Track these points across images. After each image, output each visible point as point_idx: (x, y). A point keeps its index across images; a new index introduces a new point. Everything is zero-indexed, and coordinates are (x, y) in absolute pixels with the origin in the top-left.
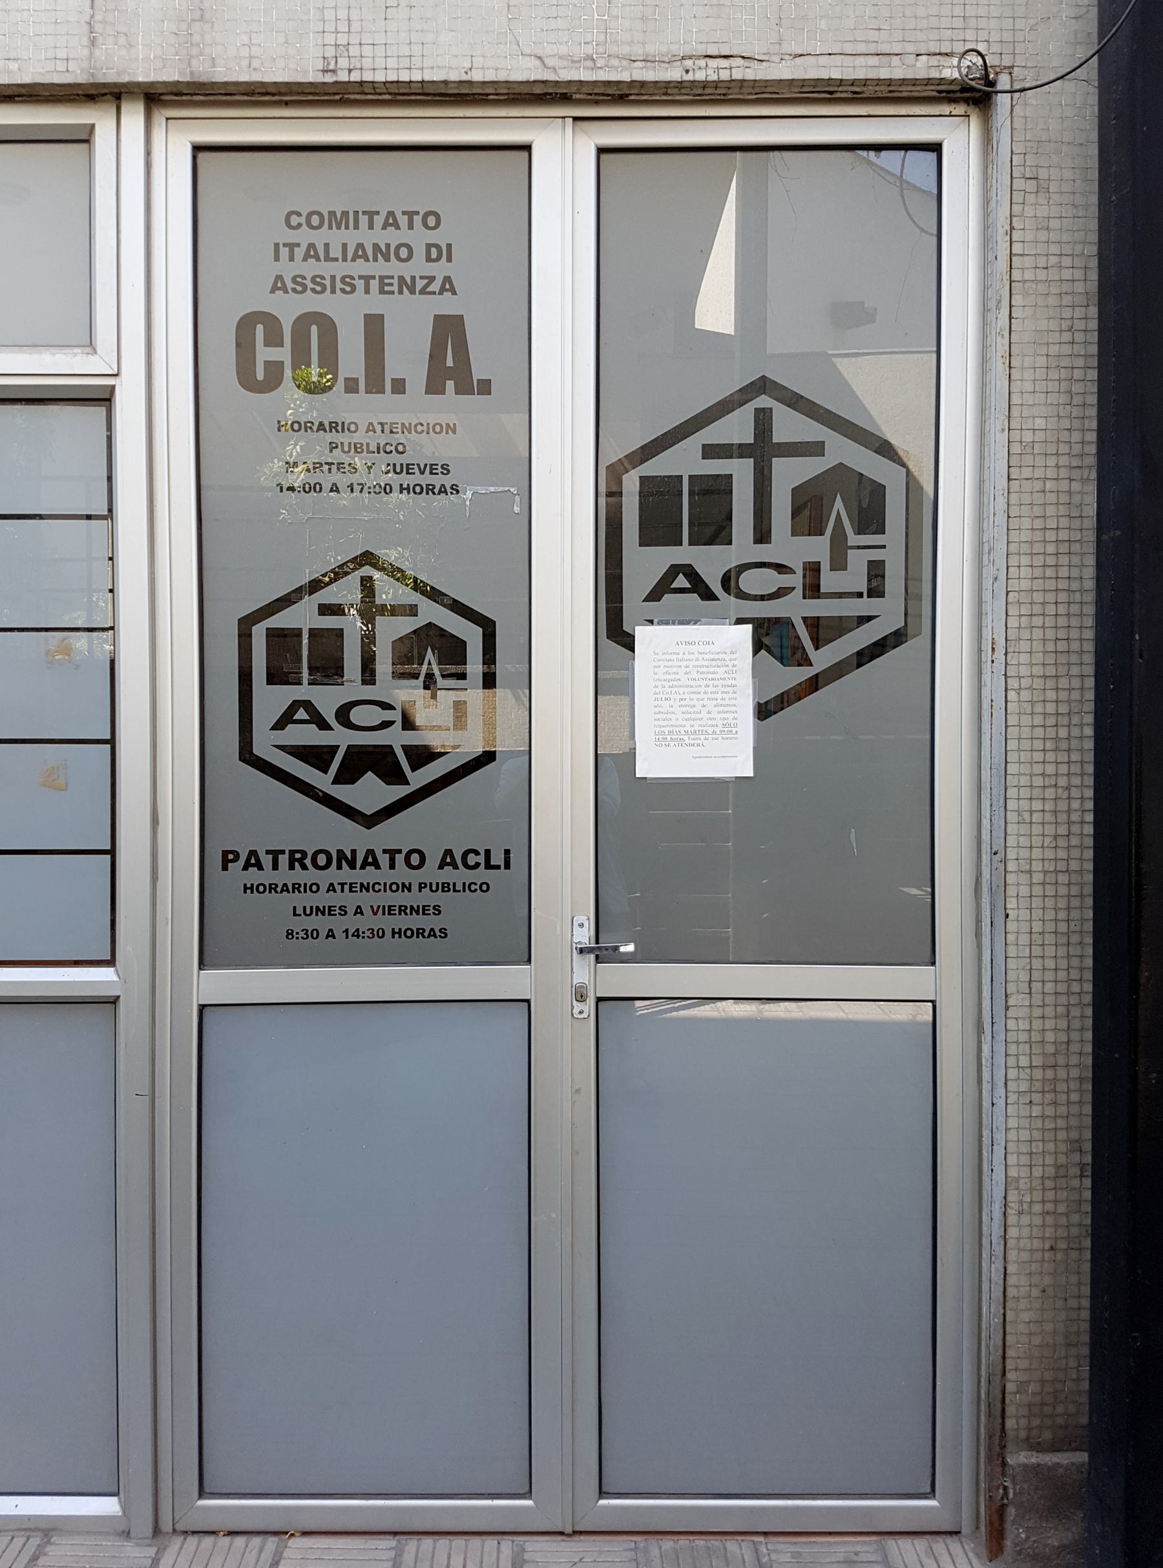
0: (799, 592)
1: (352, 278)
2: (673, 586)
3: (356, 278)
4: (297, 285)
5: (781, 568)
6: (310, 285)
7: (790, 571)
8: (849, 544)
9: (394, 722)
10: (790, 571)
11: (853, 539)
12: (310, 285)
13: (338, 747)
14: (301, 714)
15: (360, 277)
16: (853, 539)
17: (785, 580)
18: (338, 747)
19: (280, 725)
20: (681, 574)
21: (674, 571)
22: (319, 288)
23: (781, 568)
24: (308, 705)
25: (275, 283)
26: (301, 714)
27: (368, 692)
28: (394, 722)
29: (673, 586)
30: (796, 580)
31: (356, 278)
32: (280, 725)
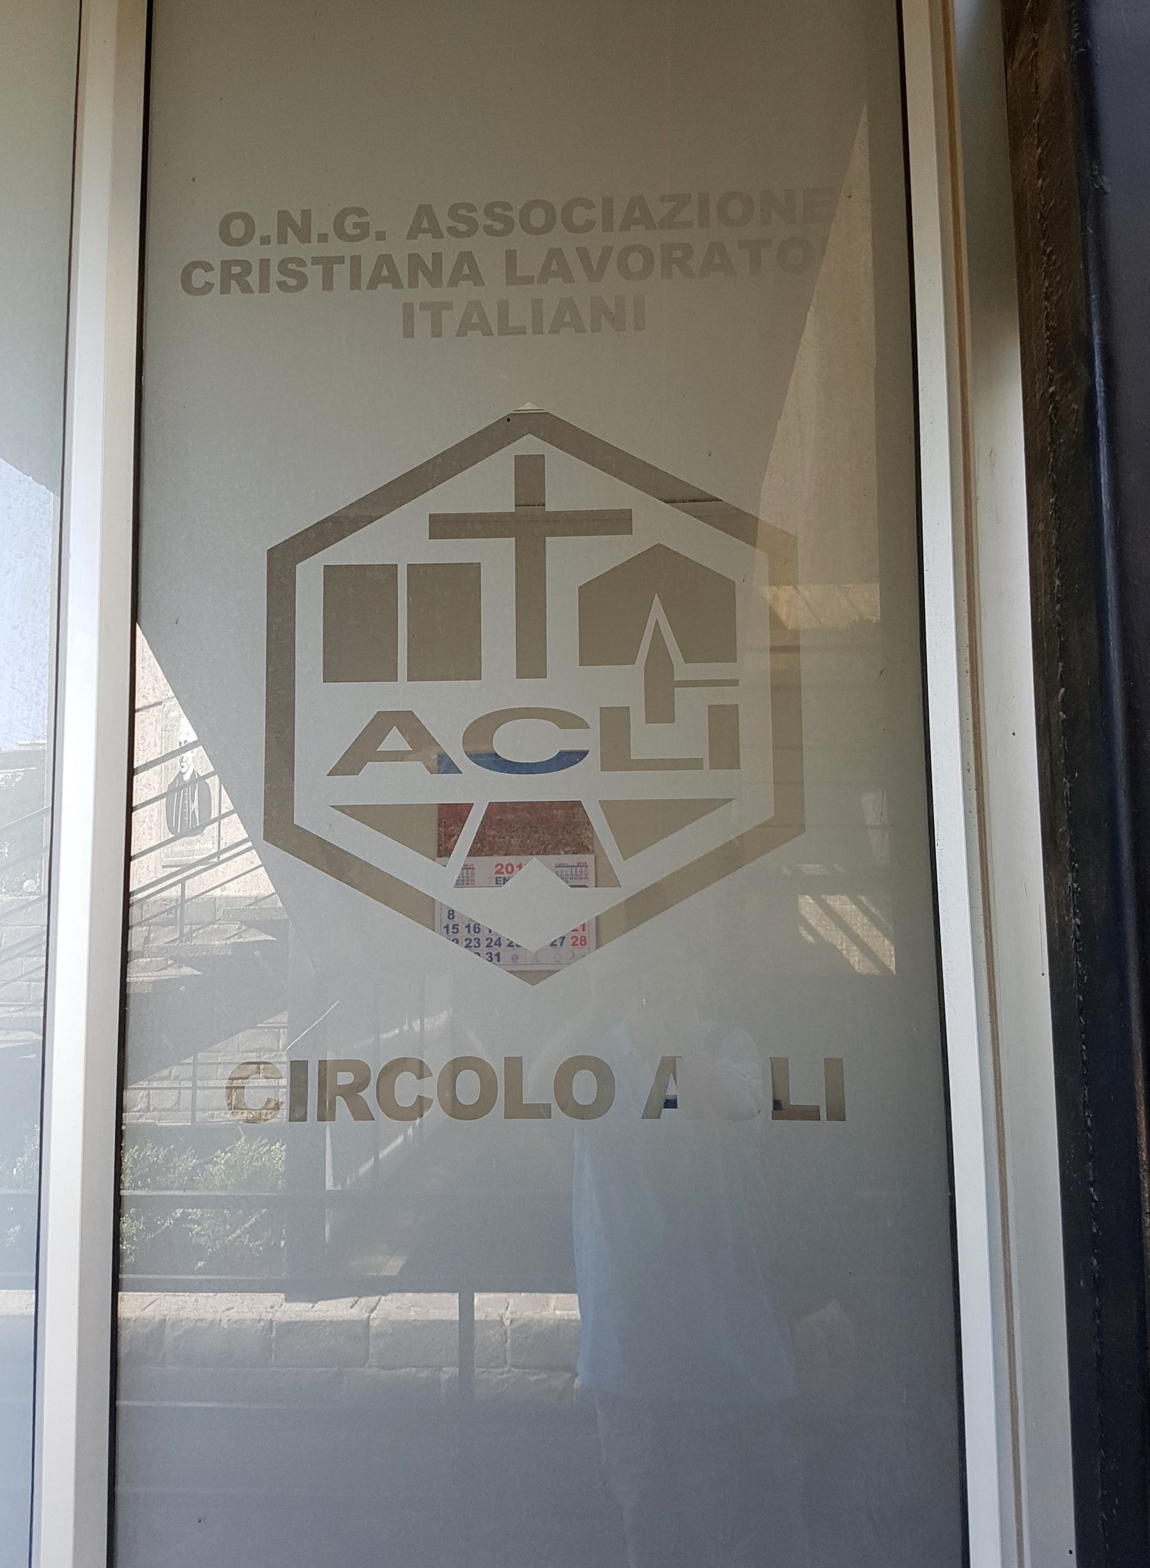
0: (593, 760)
1: (301, 263)
2: (382, 748)
3: (308, 261)
4: (458, 221)
5: (566, 720)
6: (482, 220)
7: (580, 723)
8: (676, 678)
9: (583, 754)
10: (580, 723)
11: (682, 670)
12: (482, 220)
13: (469, 807)
14: (395, 740)
15: (316, 261)
16: (682, 670)
17: (571, 740)
18: (469, 807)
19: (349, 764)
20: (395, 727)
21: (382, 723)
22: (499, 226)
23: (566, 720)
24: (407, 722)
25: (418, 219)
26: (395, 740)
27: (530, 693)
28: (583, 754)
29: (382, 748)
30: (588, 739)
31: (308, 261)
32: (349, 764)
